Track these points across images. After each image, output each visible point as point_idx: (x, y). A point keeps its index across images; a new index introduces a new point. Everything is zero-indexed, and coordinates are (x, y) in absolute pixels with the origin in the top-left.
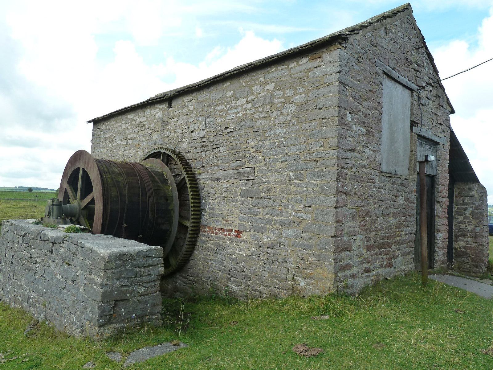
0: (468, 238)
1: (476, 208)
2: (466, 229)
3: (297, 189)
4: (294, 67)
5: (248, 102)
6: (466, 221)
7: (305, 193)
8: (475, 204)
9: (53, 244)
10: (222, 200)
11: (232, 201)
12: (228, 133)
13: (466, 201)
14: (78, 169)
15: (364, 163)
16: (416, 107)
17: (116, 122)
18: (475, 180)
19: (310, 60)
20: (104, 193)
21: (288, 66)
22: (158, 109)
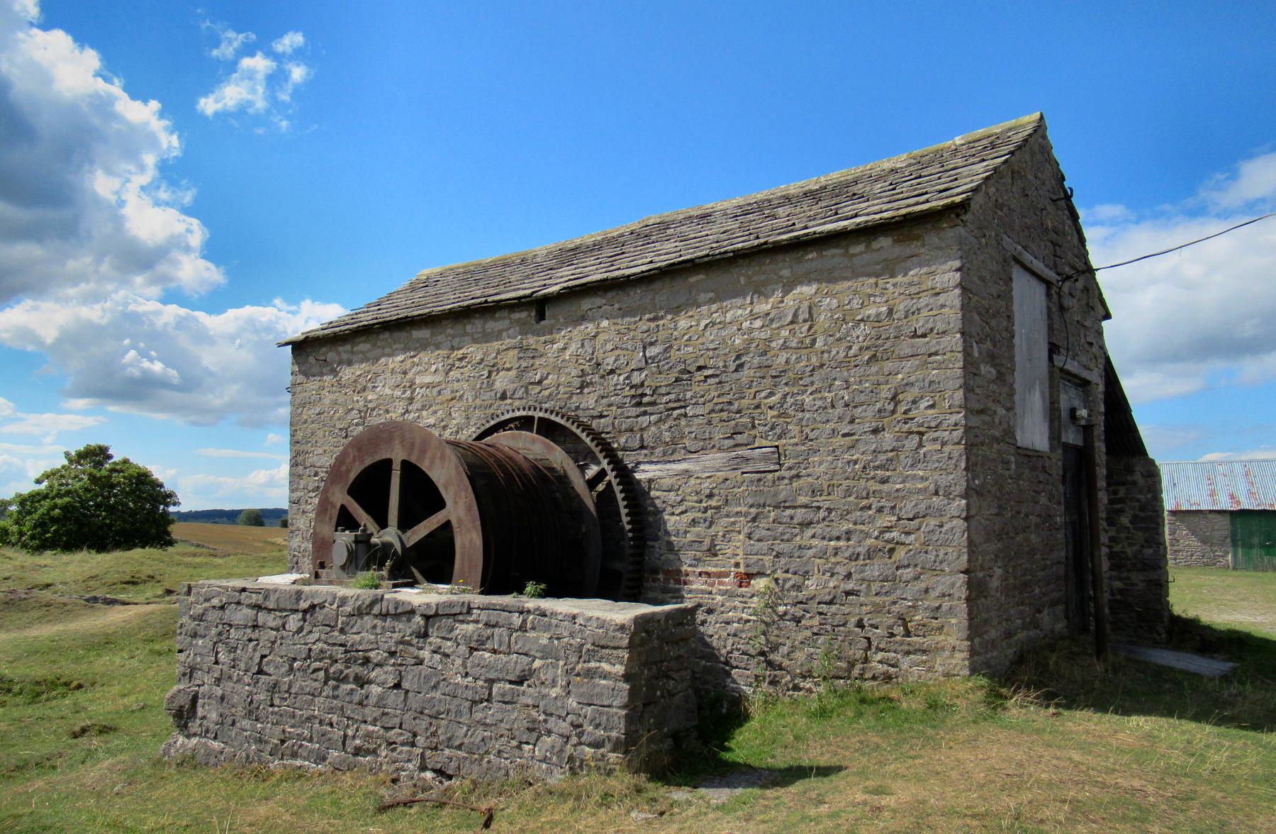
0: (1128, 571)
1: (1142, 509)
2: (1123, 552)
3: (878, 487)
4: (861, 253)
5: (753, 317)
6: (1123, 535)
7: (901, 494)
8: (1139, 500)
9: (427, 618)
10: (700, 515)
11: (727, 516)
12: (706, 377)
13: (1121, 494)
14: (387, 463)
15: (997, 434)
16: (1056, 317)
17: (374, 345)
18: (1144, 453)
19: (896, 241)
20: (1085, 503)
21: (847, 251)
22: (507, 322)
